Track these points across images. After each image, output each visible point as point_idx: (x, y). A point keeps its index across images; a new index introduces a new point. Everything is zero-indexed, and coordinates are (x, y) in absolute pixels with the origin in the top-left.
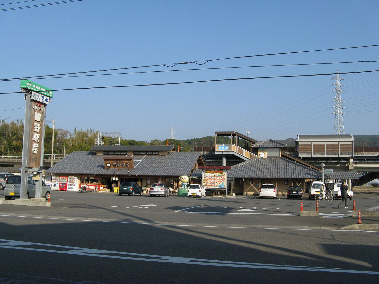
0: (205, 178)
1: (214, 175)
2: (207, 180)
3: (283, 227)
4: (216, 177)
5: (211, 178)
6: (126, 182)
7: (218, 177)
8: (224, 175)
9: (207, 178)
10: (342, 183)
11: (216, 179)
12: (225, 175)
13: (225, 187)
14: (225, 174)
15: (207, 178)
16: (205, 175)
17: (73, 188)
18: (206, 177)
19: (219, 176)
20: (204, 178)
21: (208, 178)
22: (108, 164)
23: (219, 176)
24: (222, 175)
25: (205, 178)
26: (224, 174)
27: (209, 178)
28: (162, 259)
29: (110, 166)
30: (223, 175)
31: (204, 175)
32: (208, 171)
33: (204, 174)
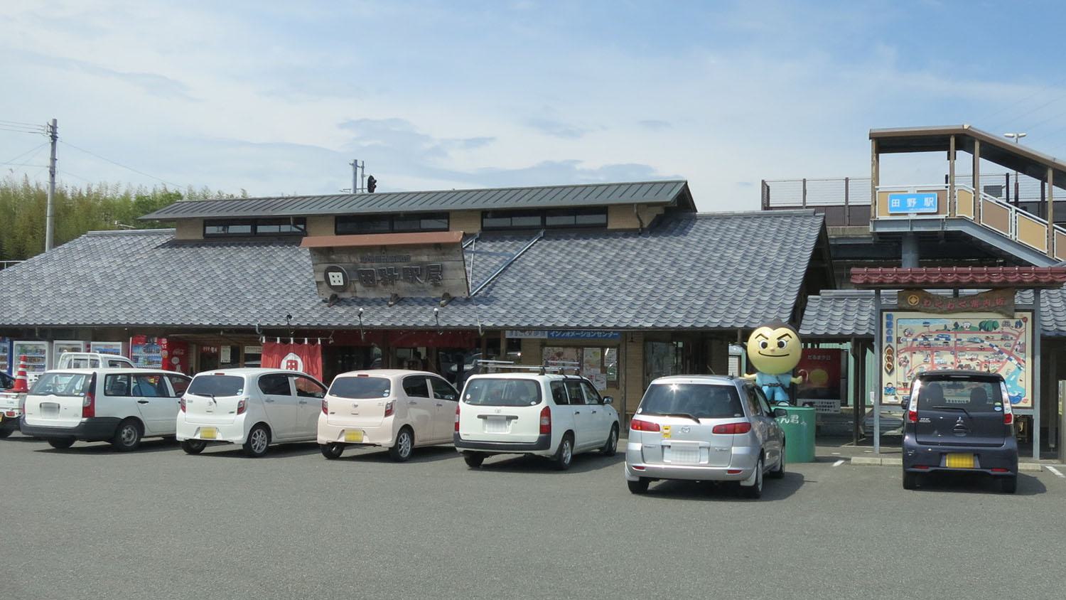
0: (894, 344)
1: (943, 325)
2: (907, 354)
3: (686, 460)
4: (965, 338)
5: (931, 340)
6: (974, 362)
7: (983, 336)
8: (1019, 324)
9: (910, 339)
10: (458, 367)
11: (963, 350)
12: (1025, 320)
13: (1029, 396)
14: (1028, 315)
15: (910, 339)
16: (894, 322)
17: (907, 191)
18: (903, 337)
19: (987, 330)
20: (889, 339)
21: (916, 343)
22: (330, 274)
23: (984, 327)
24: (1006, 324)
25: (895, 340)
26: (1018, 315)
27: (920, 339)
28: (169, 234)
29: (342, 283)
30: (1013, 322)
31: (889, 325)
32: (913, 300)
33: (889, 317)
